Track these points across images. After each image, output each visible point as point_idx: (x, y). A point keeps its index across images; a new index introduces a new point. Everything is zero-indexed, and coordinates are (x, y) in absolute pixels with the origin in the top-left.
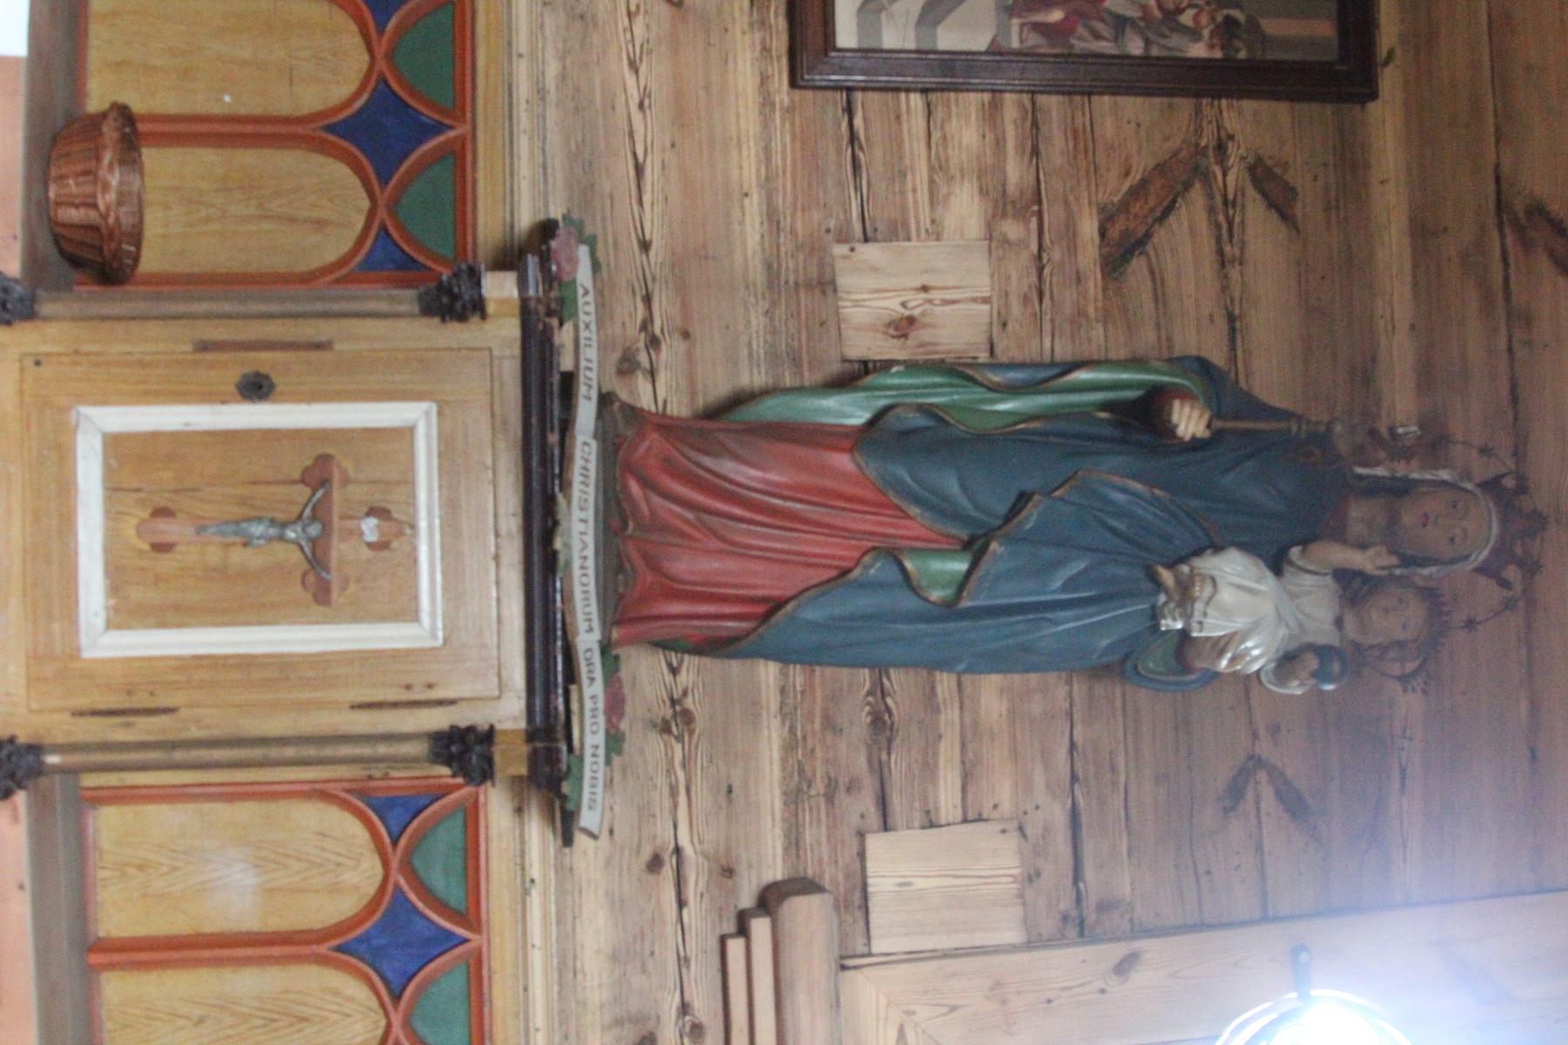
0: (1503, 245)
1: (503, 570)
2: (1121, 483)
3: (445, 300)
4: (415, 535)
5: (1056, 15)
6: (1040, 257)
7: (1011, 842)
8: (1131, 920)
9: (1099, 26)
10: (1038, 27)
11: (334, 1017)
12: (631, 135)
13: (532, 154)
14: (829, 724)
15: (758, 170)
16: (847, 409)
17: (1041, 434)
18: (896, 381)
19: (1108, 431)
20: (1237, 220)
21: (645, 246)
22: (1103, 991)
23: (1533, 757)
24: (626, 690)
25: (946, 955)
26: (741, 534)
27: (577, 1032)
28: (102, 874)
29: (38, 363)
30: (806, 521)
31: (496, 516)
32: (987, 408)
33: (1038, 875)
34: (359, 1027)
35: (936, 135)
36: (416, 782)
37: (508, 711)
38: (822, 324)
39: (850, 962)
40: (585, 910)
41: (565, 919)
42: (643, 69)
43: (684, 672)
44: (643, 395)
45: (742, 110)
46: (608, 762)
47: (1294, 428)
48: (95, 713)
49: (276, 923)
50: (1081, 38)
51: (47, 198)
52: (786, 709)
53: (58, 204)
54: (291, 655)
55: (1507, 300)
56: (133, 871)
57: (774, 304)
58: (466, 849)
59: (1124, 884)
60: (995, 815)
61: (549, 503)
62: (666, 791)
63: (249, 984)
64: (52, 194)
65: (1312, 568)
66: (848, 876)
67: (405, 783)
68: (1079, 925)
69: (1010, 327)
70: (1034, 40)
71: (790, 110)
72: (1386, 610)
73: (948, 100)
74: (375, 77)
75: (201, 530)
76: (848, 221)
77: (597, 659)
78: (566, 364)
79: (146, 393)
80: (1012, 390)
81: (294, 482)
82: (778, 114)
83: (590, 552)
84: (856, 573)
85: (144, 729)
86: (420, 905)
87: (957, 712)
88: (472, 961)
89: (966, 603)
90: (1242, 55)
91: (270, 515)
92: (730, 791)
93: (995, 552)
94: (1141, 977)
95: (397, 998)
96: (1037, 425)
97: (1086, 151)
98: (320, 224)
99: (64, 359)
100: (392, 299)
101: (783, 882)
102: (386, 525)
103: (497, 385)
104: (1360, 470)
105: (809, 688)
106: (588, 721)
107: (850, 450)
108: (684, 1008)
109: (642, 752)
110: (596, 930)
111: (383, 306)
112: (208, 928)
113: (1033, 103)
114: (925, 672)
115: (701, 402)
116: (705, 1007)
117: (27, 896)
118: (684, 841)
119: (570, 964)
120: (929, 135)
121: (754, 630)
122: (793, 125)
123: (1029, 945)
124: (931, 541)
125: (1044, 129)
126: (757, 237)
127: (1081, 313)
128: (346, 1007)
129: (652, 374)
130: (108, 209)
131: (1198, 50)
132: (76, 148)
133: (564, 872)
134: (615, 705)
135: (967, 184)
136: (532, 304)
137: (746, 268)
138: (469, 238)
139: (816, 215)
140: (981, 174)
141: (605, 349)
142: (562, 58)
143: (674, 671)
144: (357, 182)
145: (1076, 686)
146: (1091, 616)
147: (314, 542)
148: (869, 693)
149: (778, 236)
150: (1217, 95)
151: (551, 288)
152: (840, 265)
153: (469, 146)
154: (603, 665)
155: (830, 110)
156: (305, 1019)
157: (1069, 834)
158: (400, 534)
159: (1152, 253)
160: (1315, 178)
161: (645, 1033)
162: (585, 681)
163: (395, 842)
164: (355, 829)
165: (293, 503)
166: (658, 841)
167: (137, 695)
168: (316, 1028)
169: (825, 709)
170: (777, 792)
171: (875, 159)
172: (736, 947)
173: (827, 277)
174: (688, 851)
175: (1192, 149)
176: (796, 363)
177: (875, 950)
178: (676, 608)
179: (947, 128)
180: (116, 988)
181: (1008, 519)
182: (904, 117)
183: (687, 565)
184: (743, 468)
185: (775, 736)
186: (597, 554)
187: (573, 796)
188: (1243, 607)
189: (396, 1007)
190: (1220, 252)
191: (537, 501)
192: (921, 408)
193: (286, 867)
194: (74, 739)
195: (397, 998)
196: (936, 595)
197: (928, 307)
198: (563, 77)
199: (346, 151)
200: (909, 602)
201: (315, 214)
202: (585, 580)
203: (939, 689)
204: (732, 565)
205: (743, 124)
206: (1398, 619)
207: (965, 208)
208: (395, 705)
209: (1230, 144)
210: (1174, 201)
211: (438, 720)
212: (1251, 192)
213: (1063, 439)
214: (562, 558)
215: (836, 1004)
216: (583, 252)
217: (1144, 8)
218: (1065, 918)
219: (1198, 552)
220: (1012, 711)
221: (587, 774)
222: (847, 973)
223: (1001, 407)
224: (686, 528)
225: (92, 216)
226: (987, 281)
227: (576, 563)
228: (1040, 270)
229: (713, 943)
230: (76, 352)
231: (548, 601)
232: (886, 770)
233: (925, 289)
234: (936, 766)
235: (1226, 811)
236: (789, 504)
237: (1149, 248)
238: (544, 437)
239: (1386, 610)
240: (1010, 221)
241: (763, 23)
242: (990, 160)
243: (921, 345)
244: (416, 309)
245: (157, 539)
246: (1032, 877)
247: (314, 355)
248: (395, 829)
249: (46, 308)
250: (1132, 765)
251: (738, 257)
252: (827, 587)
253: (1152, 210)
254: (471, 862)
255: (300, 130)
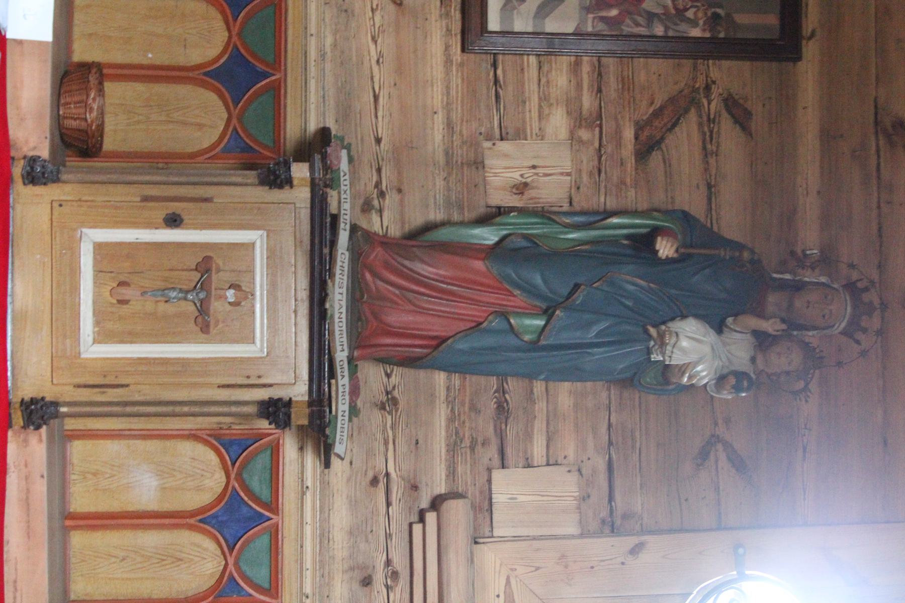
0: (877, 146)
1: (298, 318)
2: (631, 280)
3: (272, 178)
4: (254, 299)
5: (614, 12)
6: (600, 150)
7: (573, 478)
8: (642, 525)
9: (640, 19)
10: (602, 19)
11: (196, 559)
12: (372, 78)
13: (317, 91)
14: (474, 408)
15: (442, 99)
16: (486, 235)
17: (590, 252)
18: (513, 221)
19: (628, 252)
20: (715, 130)
21: (378, 141)
22: (623, 563)
23: (885, 443)
24: (361, 384)
25: (534, 538)
26: (424, 302)
27: (329, 573)
28: (73, 477)
29: (61, 205)
30: (460, 297)
31: (295, 290)
32: (562, 237)
33: (589, 497)
34: (209, 565)
35: (544, 80)
36: (246, 432)
37: (299, 391)
38: (475, 186)
39: (481, 540)
40: (336, 506)
41: (325, 510)
42: (379, 41)
43: (394, 376)
44: (375, 224)
45: (434, 65)
46: (350, 420)
47: (723, 253)
48: (86, 386)
49: (167, 507)
50: (628, 26)
51: (59, 115)
52: (450, 399)
53: (65, 118)
54: (188, 359)
55: (879, 177)
56: (90, 476)
57: (449, 174)
58: (271, 469)
59: (638, 503)
60: (565, 462)
61: (323, 284)
62: (382, 441)
63: (151, 539)
64: (61, 113)
65: (738, 329)
66: (481, 492)
67: (239, 432)
68: (611, 526)
69: (581, 189)
70: (601, 27)
71: (461, 65)
72: (779, 354)
73: (551, 60)
74: (232, 45)
75: (143, 294)
76: (493, 128)
77: (346, 366)
78: (333, 209)
79: (117, 222)
80: (577, 227)
81: (191, 270)
82: (454, 68)
83: (344, 310)
84: (485, 325)
85: (112, 395)
86: (246, 498)
87: (545, 404)
88: (273, 530)
89: (543, 342)
90: (722, 35)
91: (179, 287)
92: (417, 443)
93: (558, 316)
94: (645, 557)
95: (231, 549)
96: (586, 247)
97: (629, 90)
98: (200, 126)
99: (74, 203)
100: (244, 176)
101: (445, 494)
102: (239, 293)
103: (297, 222)
104: (775, 275)
105: (463, 387)
106: (340, 398)
107: (483, 259)
108: (388, 562)
109: (369, 420)
110: (341, 518)
111: (239, 180)
112: (131, 508)
113: (599, 62)
114: (527, 381)
115: (407, 228)
116: (400, 562)
117: (45, 481)
118: (391, 469)
119: (327, 535)
120: (540, 80)
121: (429, 354)
122: (462, 75)
123: (582, 536)
124: (527, 309)
125: (605, 77)
126: (441, 137)
127: (623, 182)
128: (200, 561)
129: (380, 211)
130: (92, 122)
131: (696, 33)
132: (74, 87)
133: (325, 484)
134: (355, 391)
135: (559, 109)
136: (317, 181)
137: (434, 153)
138: (282, 136)
139: (474, 125)
140: (568, 102)
141: (355, 198)
142: (335, 34)
143: (388, 376)
144: (221, 103)
145: (613, 392)
146: (613, 351)
147: (202, 301)
148: (495, 392)
149: (452, 137)
150: (706, 58)
151: (327, 174)
152: (487, 152)
153: (283, 85)
154: (349, 369)
155: (484, 65)
156: (181, 560)
157: (607, 475)
158: (246, 298)
159: (664, 149)
160: (764, 105)
161: (366, 575)
162: (340, 377)
163: (233, 464)
164: (211, 457)
165: (190, 280)
166: (377, 469)
167: (108, 378)
168: (186, 565)
169: (471, 400)
170: (443, 445)
171: (508, 94)
172: (417, 529)
173: (480, 160)
174: (393, 475)
175: (691, 89)
176: (461, 208)
177: (495, 534)
178: (389, 341)
179: (549, 76)
180: (78, 539)
181: (568, 298)
182: (526, 70)
183: (396, 318)
184: (426, 267)
185: (443, 413)
186: (347, 312)
187: (331, 436)
188: (693, 348)
189: (231, 554)
190: (704, 148)
191: (317, 282)
192: (526, 237)
193: (174, 476)
194: (75, 399)
195: (231, 549)
196: (527, 338)
197: (535, 177)
198: (335, 45)
199: (220, 90)
200: (512, 341)
201: (198, 120)
202: (341, 324)
203: (535, 390)
204: (420, 318)
205: (435, 73)
206: (786, 359)
207: (558, 122)
208: (241, 386)
209: (713, 86)
210: (679, 119)
211: (263, 394)
212: (725, 114)
213: (603, 254)
214: (329, 312)
215: (471, 560)
216: (344, 153)
217: (665, 7)
218: (603, 522)
219: (673, 319)
220: (576, 405)
221: (339, 425)
222: (478, 546)
223: (571, 236)
224: (395, 299)
225: (83, 125)
226: (569, 163)
227: (337, 316)
228: (600, 157)
229: (406, 527)
230: (80, 200)
231: (321, 335)
232: (504, 434)
233: (534, 167)
234: (532, 431)
235: (698, 465)
236: (449, 287)
237: (663, 146)
238: (321, 250)
239: (779, 354)
240: (583, 130)
241: (447, 14)
242: (573, 94)
243: (531, 199)
244: (256, 181)
245: (120, 298)
246: (585, 498)
247: (205, 205)
248: (234, 457)
249: (64, 177)
250: (644, 437)
251: (430, 148)
252: (470, 331)
253: (665, 125)
254: (274, 476)
255: (191, 74)
